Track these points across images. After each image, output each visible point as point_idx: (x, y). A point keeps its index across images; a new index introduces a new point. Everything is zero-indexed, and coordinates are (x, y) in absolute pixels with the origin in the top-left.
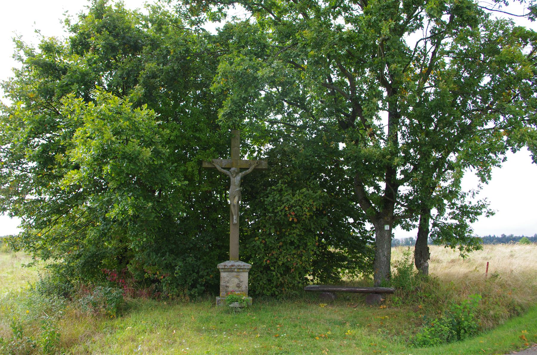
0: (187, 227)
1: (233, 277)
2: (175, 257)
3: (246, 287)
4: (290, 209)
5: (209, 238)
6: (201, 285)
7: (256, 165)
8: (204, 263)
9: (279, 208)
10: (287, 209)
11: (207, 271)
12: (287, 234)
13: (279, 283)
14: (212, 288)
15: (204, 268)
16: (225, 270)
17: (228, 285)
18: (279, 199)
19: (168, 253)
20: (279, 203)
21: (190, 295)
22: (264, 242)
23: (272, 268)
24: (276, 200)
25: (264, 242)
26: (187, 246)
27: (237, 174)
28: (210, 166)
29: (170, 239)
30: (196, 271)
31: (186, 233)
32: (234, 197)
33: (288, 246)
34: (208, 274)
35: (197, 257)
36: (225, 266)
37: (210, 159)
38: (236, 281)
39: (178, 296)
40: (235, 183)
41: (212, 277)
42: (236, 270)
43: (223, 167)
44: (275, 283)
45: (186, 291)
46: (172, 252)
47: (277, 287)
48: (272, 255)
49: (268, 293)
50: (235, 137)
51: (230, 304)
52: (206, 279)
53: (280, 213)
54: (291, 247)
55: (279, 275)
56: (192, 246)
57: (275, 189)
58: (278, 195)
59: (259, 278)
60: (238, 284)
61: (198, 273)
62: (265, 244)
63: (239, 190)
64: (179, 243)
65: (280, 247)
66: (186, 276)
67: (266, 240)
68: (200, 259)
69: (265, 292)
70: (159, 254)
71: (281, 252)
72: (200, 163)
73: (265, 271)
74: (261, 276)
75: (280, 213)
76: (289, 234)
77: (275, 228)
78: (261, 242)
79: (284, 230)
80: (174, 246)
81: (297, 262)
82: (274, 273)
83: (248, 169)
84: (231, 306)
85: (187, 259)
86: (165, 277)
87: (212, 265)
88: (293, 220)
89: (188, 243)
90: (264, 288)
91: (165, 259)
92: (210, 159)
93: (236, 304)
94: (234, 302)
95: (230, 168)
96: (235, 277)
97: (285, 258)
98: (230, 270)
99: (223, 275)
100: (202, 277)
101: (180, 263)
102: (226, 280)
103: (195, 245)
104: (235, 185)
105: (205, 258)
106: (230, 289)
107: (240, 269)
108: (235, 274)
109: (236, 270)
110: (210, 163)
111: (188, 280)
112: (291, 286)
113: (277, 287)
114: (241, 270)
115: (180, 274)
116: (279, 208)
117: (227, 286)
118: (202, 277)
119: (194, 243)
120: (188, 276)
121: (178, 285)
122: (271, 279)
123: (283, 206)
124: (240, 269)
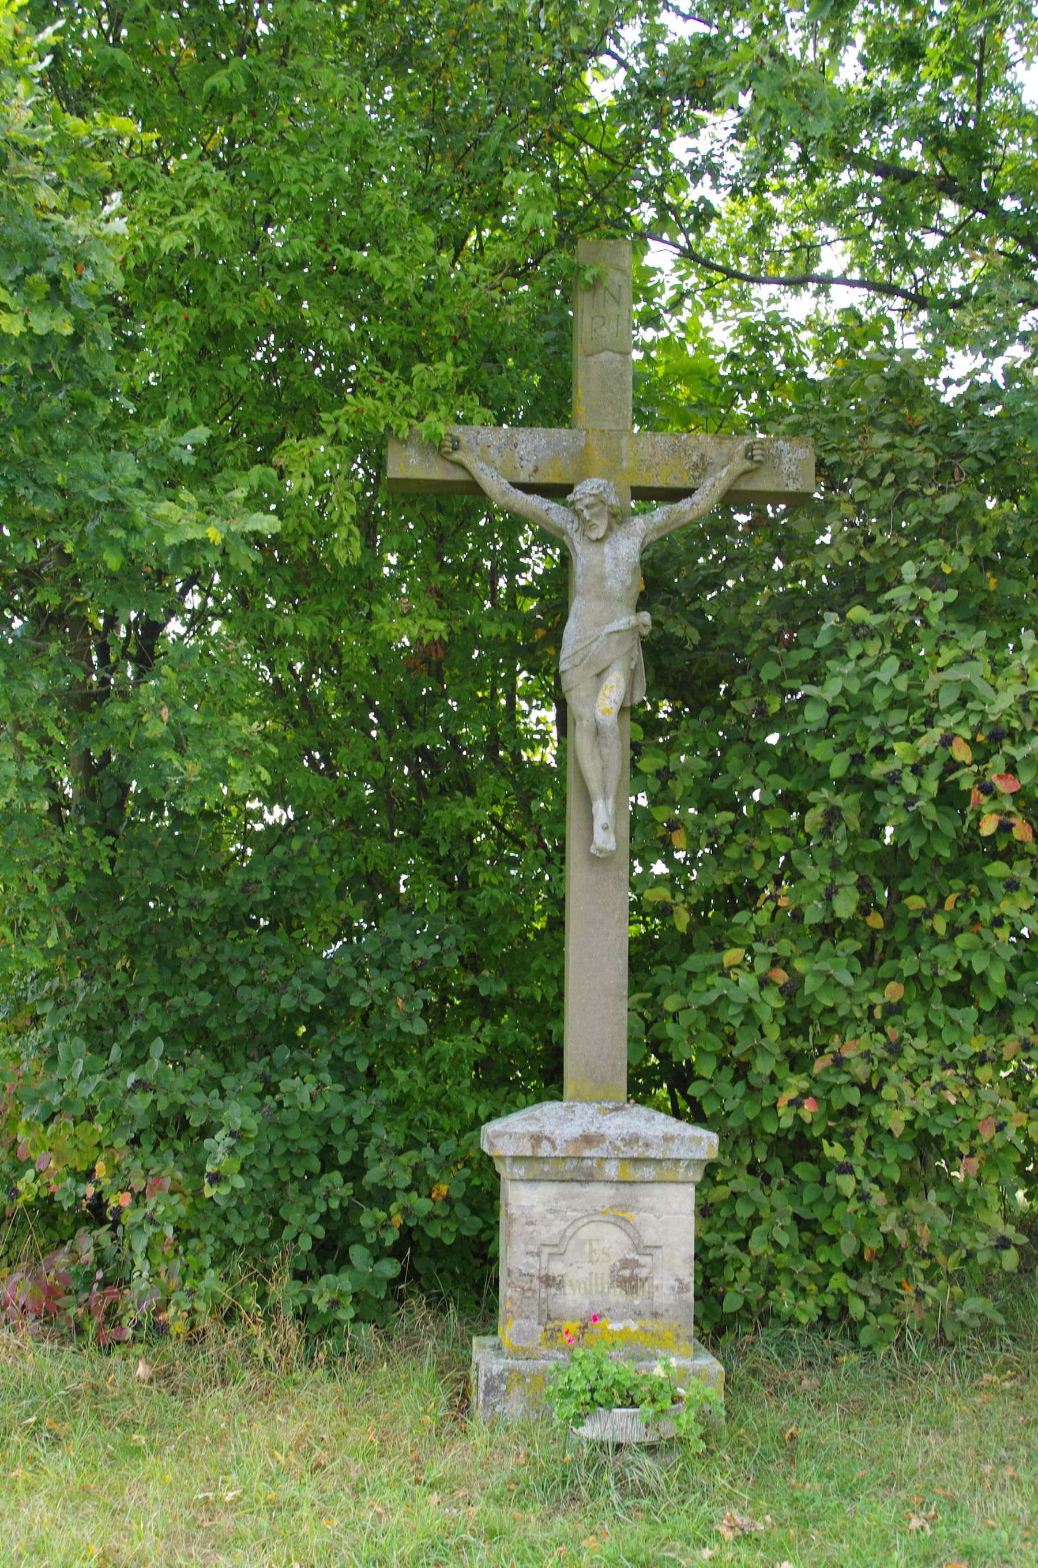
0: (288, 879)
1: (592, 1215)
2: (216, 1070)
3: (682, 1288)
4: (983, 754)
5: (425, 951)
6: (379, 1252)
7: (739, 464)
8: (399, 1104)
9: (900, 748)
10: (962, 753)
11: (412, 1157)
12: (940, 925)
13: (874, 1243)
14: (455, 1268)
15: (396, 1139)
16: (539, 1167)
17: (556, 1268)
18: (902, 684)
19: (157, 1047)
20: (897, 716)
21: (305, 1313)
22: (781, 977)
23: (835, 1152)
24: (880, 697)
25: (781, 977)
26: (287, 1002)
27: (618, 518)
28: (436, 471)
29: (182, 952)
30: (344, 1157)
31: (285, 920)
32: (600, 675)
33: (937, 1004)
34: (419, 1181)
35: (352, 1068)
36: (537, 1139)
37: (436, 424)
38: (613, 1242)
39: (230, 1316)
40: (602, 578)
41: (448, 1199)
42: (611, 1170)
43: (523, 478)
44: (847, 1246)
45: (283, 1289)
46: (192, 1033)
47: (854, 1269)
48: (839, 1062)
49: (808, 1311)
50: (597, 280)
51: (579, 1419)
52: (406, 1211)
53: (910, 784)
54: (956, 1014)
55: (878, 1197)
56: (316, 997)
57: (874, 620)
58: (893, 663)
59: (743, 1211)
60: (626, 1263)
61: (354, 1170)
62: (790, 992)
63: (634, 629)
64: (235, 980)
65: (893, 1009)
66: (281, 1186)
67: (799, 965)
68: (372, 1079)
69: (785, 1299)
70: (115, 1050)
71: (895, 1049)
72: (373, 448)
73: (775, 1166)
74: (758, 1194)
75: (910, 784)
76: (954, 931)
77: (863, 885)
78: (764, 983)
79: (915, 903)
80: (204, 999)
81: (998, 1110)
82: (847, 1184)
83: (687, 493)
84: (589, 1431)
85: (286, 1084)
86: (150, 1201)
87: (445, 1122)
88: (1005, 828)
89: (297, 983)
90: (772, 1269)
91: (141, 1085)
92: (436, 424)
93: (619, 1424)
94: (608, 1405)
95: (569, 489)
96: (601, 1210)
97: (925, 1088)
98: (574, 1169)
99: (522, 1200)
100: (383, 1197)
101: (238, 1114)
102: (545, 1234)
103: (339, 997)
104: (604, 597)
105: (399, 1074)
106: (573, 1299)
107: (636, 1161)
108: (601, 1194)
109: (611, 1170)
110: (440, 448)
111: (295, 1217)
112: (951, 1264)
113: (854, 1269)
114: (648, 1172)
115: (240, 1182)
116: (900, 748)
117: (548, 1281)
118: (383, 1197)
119: (332, 982)
120: (293, 1189)
121: (229, 1244)
122: (819, 1213)
123: (935, 734)
124: (641, 1164)
